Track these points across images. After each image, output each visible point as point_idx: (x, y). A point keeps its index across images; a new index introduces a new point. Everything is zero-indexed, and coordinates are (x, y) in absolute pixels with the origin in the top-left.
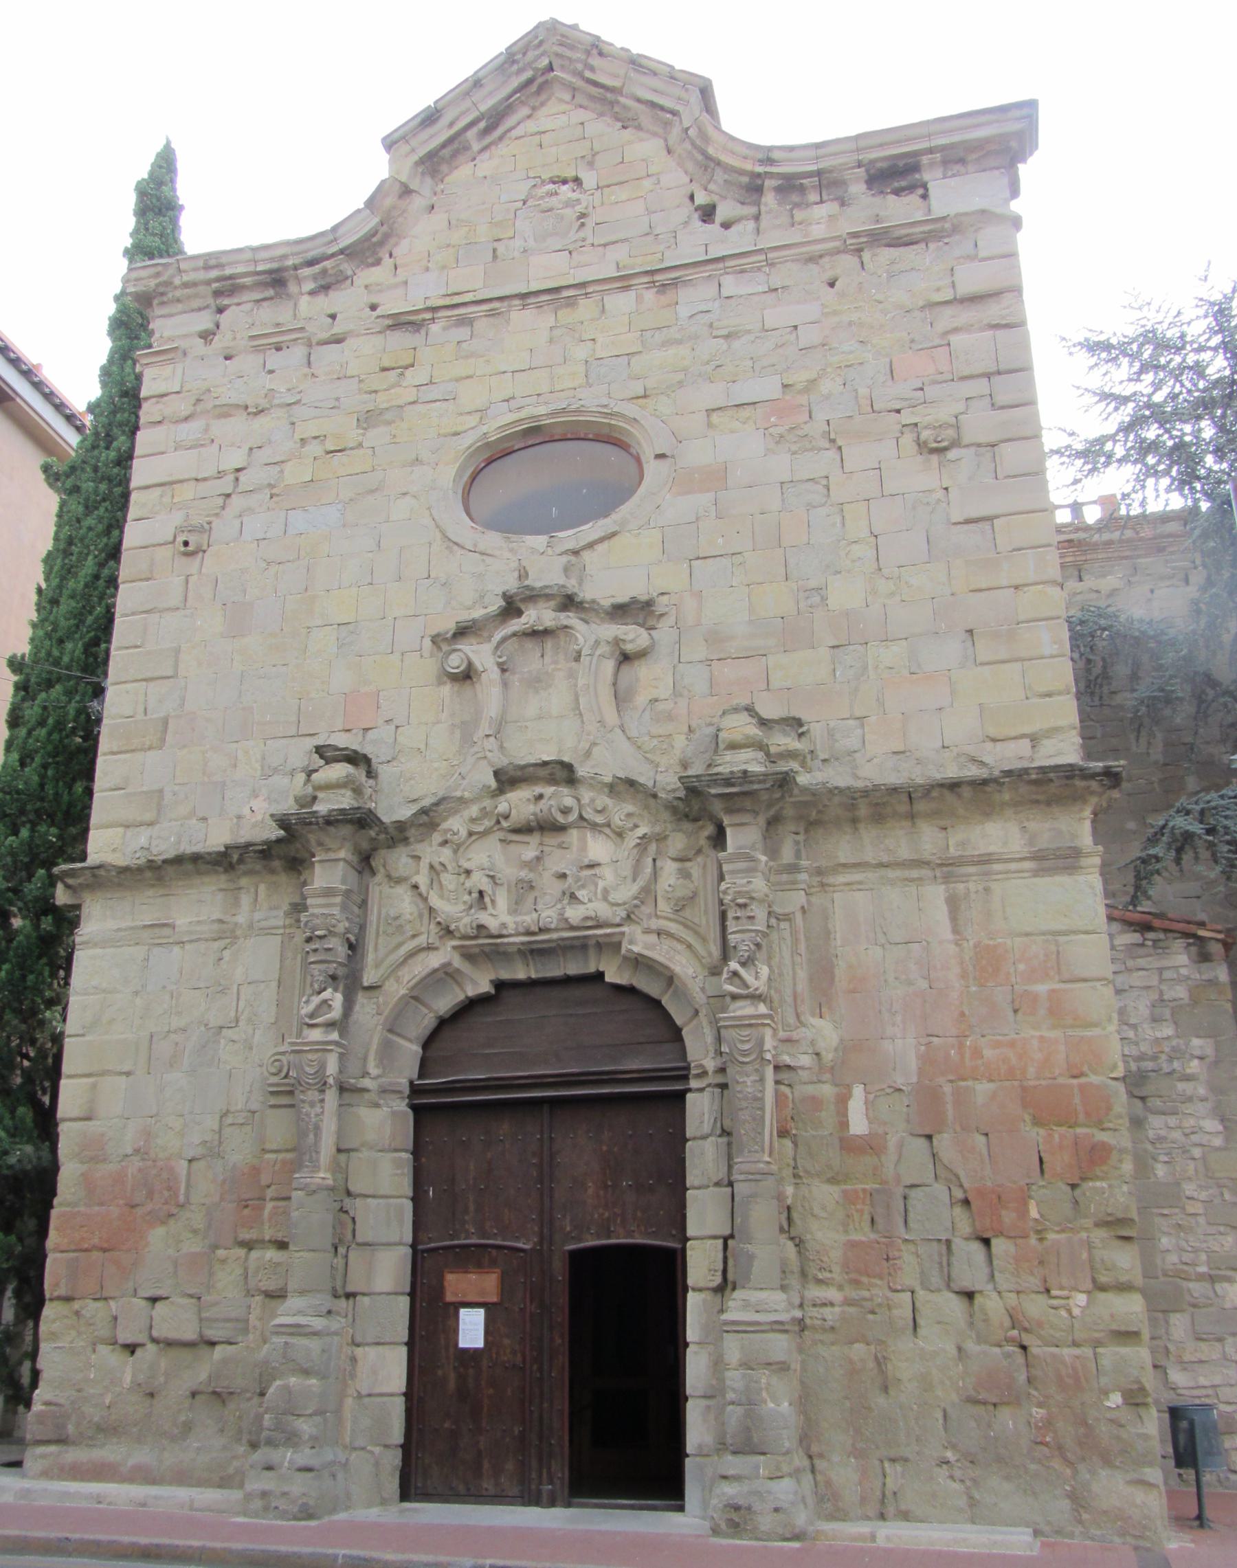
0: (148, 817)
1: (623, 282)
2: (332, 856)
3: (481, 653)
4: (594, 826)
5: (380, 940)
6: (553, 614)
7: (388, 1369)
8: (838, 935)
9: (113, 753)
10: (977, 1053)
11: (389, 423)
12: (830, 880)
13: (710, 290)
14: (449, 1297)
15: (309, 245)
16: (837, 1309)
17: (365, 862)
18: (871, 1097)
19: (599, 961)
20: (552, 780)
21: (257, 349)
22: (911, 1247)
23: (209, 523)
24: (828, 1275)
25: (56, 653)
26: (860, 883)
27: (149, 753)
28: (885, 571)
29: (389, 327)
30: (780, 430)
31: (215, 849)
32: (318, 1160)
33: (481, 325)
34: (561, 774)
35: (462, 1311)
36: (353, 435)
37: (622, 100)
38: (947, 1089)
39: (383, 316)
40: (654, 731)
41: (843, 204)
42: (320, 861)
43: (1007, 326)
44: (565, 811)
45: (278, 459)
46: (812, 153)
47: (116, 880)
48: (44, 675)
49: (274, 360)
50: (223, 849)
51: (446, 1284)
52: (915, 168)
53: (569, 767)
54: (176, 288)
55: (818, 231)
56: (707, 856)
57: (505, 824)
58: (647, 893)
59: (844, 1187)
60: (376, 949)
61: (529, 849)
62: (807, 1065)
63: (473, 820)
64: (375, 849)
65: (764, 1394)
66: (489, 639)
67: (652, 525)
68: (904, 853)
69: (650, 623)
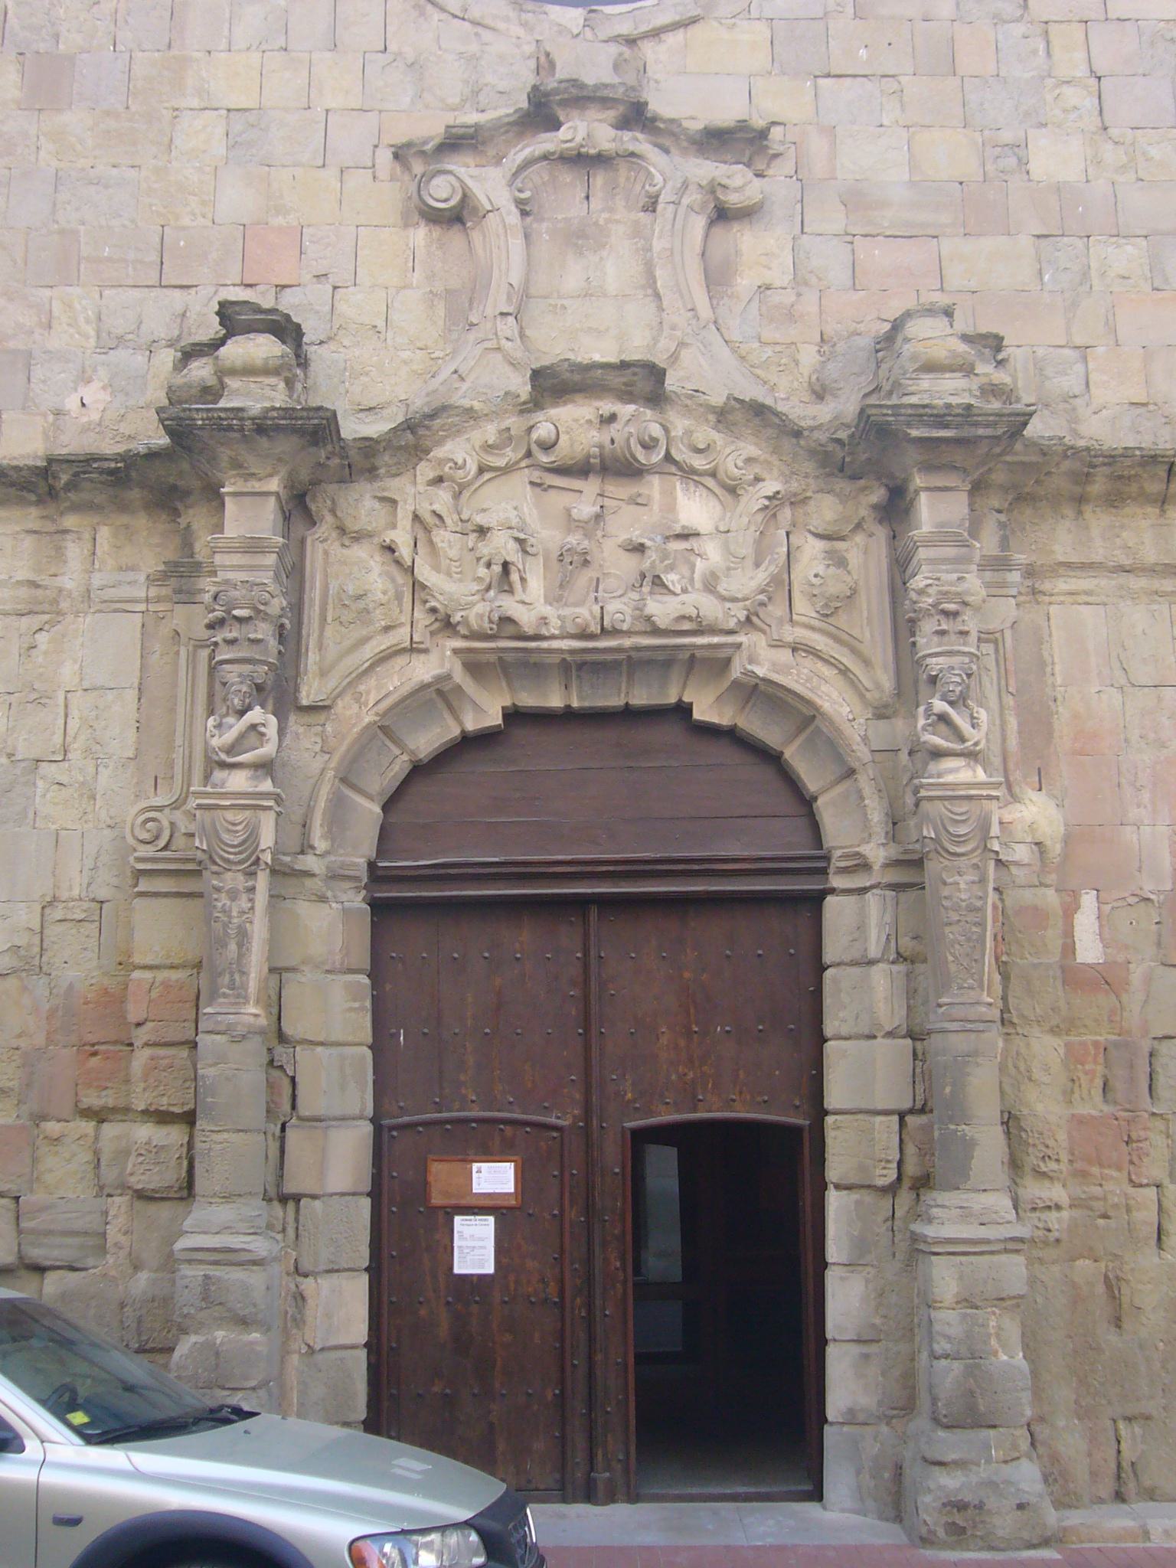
3: (488, 183)
4: (689, 473)
5: (329, 632)
6: (612, 132)
7: (343, 1309)
8: (1057, 668)
12: (1046, 586)
14: (437, 1200)
16: (1065, 1214)
17: (298, 506)
18: (1107, 908)
20: (627, 395)
22: (1159, 1124)
24: (1053, 1165)
26: (1087, 593)
28: (1114, 132)
32: (244, 986)
34: (643, 386)
35: (458, 1220)
40: (768, 334)
44: (648, 445)
51: (431, 1179)
53: (656, 373)
57: (544, 459)
58: (782, 585)
59: (1072, 1038)
60: (321, 647)
61: (585, 498)
62: (1026, 861)
64: (315, 483)
65: (993, 1342)
67: (754, 14)
69: (760, 165)
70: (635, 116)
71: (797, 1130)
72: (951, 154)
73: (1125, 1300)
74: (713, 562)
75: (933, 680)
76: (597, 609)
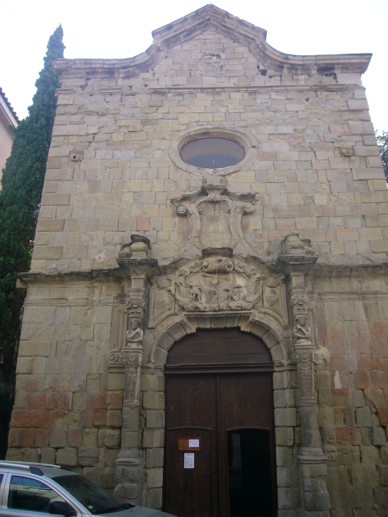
0: (57, 256)
1: (237, 89)
2: (139, 277)
3: (192, 207)
4: (239, 273)
5: (155, 310)
6: (220, 196)
7: (157, 477)
8: (327, 317)
9: (42, 231)
10: (377, 360)
11: (153, 124)
12: (323, 297)
13: (268, 97)
14: (180, 449)
15: (125, 61)
16: (336, 453)
17: (149, 281)
18: (342, 375)
19: (239, 323)
20: (224, 255)
21: (102, 94)
22: (358, 429)
23: (83, 151)
24: (332, 440)
25: (15, 193)
27: (57, 232)
28: (334, 193)
29: (153, 93)
30: (294, 144)
31: (87, 271)
33: (186, 96)
34: (228, 253)
36: (139, 127)
37: (234, 33)
38: (368, 372)
39: (151, 89)
40: (256, 241)
41: (309, 76)
42: (133, 279)
43: (366, 121)
45: (110, 132)
46: (301, 58)
47: (44, 280)
48: (10, 201)
49: (108, 98)
50: (90, 271)
51: (179, 443)
52: (333, 68)
53: (231, 250)
54: (73, 69)
55: (302, 83)
56: (281, 286)
57: (205, 270)
58: (261, 298)
59: (335, 408)
61: (215, 279)
63: (192, 268)
64: (152, 276)
66: (194, 202)
67: (251, 169)
68: (347, 289)
70: (225, 192)
71: (268, 431)
72: (297, 199)
73: (353, 476)
74: (243, 292)
75: (297, 320)
76: (218, 305)
